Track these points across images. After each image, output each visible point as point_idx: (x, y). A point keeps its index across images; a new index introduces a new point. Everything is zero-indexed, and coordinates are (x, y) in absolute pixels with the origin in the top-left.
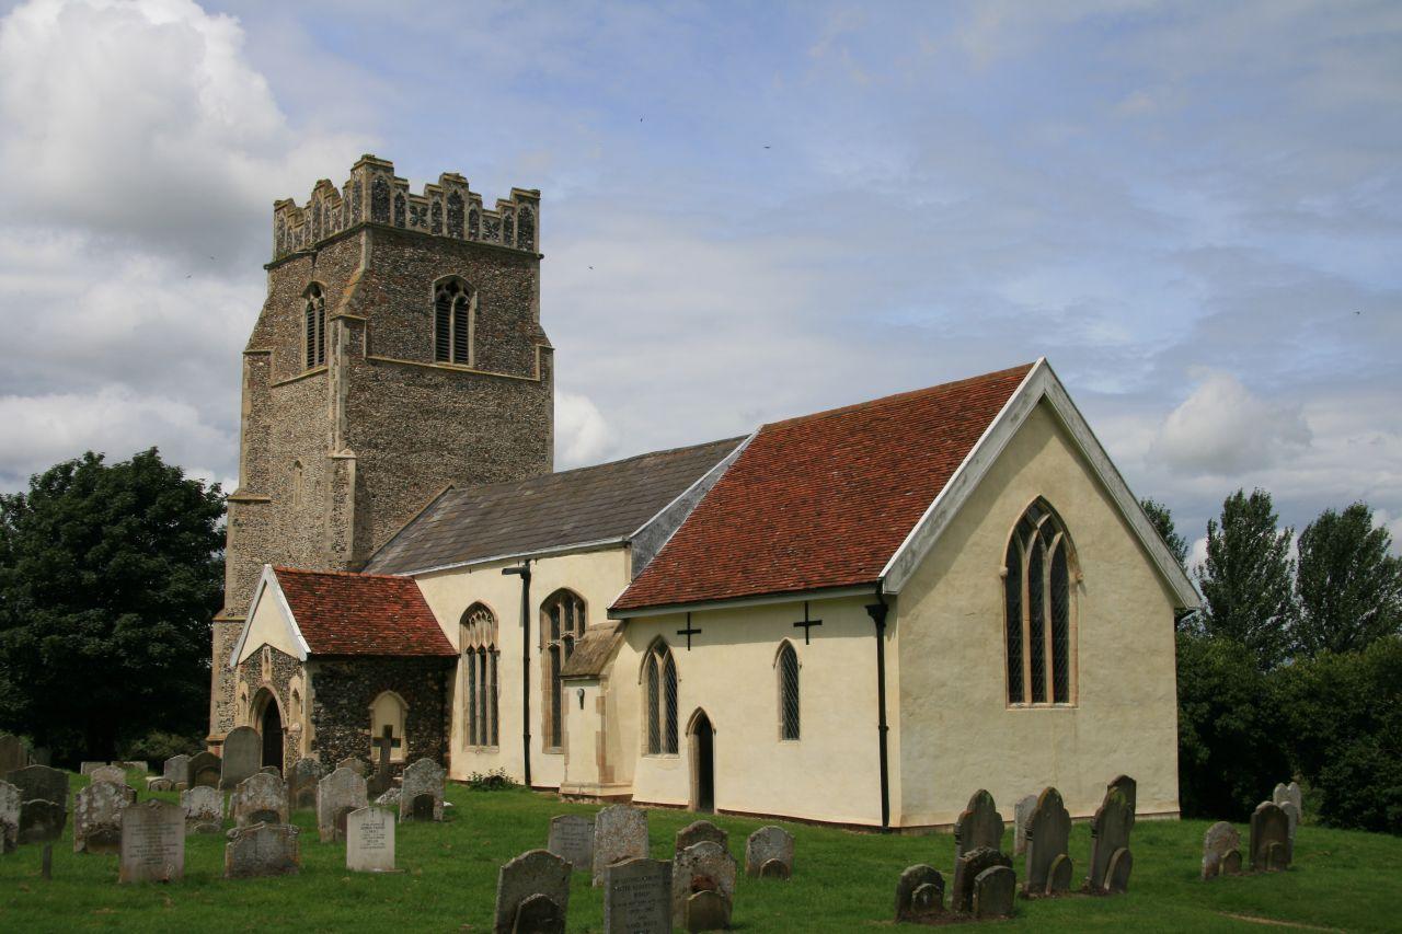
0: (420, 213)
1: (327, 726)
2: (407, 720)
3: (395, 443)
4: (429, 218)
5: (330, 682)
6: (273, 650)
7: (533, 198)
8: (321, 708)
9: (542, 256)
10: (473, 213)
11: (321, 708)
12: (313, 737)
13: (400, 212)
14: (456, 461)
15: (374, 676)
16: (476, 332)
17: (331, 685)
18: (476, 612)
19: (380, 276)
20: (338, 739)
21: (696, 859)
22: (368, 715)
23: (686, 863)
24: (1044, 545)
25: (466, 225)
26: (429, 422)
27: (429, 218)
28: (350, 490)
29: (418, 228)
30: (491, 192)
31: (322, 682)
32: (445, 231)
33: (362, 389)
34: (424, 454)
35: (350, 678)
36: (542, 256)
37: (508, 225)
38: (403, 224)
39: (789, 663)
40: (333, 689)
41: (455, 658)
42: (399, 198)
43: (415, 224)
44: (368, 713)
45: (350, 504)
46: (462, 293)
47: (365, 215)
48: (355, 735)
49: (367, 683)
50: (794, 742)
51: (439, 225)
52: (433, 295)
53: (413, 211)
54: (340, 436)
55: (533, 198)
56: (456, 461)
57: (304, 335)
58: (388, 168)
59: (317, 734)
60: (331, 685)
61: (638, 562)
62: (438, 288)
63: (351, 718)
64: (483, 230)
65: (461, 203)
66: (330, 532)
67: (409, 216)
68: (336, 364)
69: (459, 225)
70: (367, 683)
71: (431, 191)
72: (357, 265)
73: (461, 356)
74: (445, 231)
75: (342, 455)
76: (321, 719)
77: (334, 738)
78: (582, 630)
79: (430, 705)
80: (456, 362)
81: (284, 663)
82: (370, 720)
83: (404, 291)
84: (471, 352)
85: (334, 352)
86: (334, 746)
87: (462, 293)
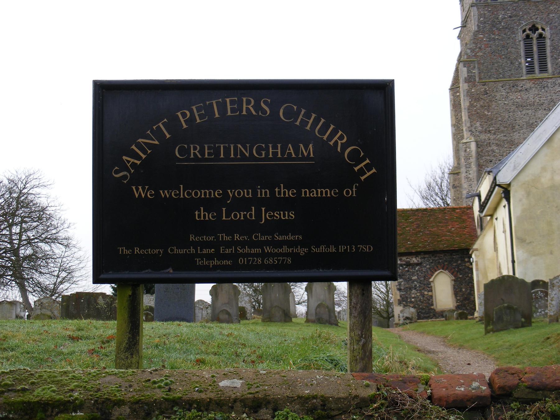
1: (406, 291)
2: (454, 286)
3: (502, 128)
5: (406, 268)
8: (402, 282)
11: (402, 282)
12: (399, 298)
15: (432, 263)
16: (551, 52)
17: (407, 269)
19: (483, 32)
20: (413, 298)
21: (42, 303)
22: (430, 284)
23: (38, 305)
26: (524, 112)
28: (473, 160)
31: (401, 268)
33: (477, 100)
34: (521, 131)
35: (417, 264)
40: (408, 271)
44: (429, 283)
46: (540, 31)
48: (423, 295)
49: (428, 266)
52: (520, 36)
54: (466, 129)
59: (401, 296)
60: (407, 269)
62: (524, 31)
63: (420, 286)
70: (428, 266)
73: (543, 68)
75: (468, 140)
76: (402, 288)
77: (411, 298)
79: (468, 276)
80: (540, 73)
82: (431, 287)
83: (500, 38)
84: (549, 65)
87: (540, 31)
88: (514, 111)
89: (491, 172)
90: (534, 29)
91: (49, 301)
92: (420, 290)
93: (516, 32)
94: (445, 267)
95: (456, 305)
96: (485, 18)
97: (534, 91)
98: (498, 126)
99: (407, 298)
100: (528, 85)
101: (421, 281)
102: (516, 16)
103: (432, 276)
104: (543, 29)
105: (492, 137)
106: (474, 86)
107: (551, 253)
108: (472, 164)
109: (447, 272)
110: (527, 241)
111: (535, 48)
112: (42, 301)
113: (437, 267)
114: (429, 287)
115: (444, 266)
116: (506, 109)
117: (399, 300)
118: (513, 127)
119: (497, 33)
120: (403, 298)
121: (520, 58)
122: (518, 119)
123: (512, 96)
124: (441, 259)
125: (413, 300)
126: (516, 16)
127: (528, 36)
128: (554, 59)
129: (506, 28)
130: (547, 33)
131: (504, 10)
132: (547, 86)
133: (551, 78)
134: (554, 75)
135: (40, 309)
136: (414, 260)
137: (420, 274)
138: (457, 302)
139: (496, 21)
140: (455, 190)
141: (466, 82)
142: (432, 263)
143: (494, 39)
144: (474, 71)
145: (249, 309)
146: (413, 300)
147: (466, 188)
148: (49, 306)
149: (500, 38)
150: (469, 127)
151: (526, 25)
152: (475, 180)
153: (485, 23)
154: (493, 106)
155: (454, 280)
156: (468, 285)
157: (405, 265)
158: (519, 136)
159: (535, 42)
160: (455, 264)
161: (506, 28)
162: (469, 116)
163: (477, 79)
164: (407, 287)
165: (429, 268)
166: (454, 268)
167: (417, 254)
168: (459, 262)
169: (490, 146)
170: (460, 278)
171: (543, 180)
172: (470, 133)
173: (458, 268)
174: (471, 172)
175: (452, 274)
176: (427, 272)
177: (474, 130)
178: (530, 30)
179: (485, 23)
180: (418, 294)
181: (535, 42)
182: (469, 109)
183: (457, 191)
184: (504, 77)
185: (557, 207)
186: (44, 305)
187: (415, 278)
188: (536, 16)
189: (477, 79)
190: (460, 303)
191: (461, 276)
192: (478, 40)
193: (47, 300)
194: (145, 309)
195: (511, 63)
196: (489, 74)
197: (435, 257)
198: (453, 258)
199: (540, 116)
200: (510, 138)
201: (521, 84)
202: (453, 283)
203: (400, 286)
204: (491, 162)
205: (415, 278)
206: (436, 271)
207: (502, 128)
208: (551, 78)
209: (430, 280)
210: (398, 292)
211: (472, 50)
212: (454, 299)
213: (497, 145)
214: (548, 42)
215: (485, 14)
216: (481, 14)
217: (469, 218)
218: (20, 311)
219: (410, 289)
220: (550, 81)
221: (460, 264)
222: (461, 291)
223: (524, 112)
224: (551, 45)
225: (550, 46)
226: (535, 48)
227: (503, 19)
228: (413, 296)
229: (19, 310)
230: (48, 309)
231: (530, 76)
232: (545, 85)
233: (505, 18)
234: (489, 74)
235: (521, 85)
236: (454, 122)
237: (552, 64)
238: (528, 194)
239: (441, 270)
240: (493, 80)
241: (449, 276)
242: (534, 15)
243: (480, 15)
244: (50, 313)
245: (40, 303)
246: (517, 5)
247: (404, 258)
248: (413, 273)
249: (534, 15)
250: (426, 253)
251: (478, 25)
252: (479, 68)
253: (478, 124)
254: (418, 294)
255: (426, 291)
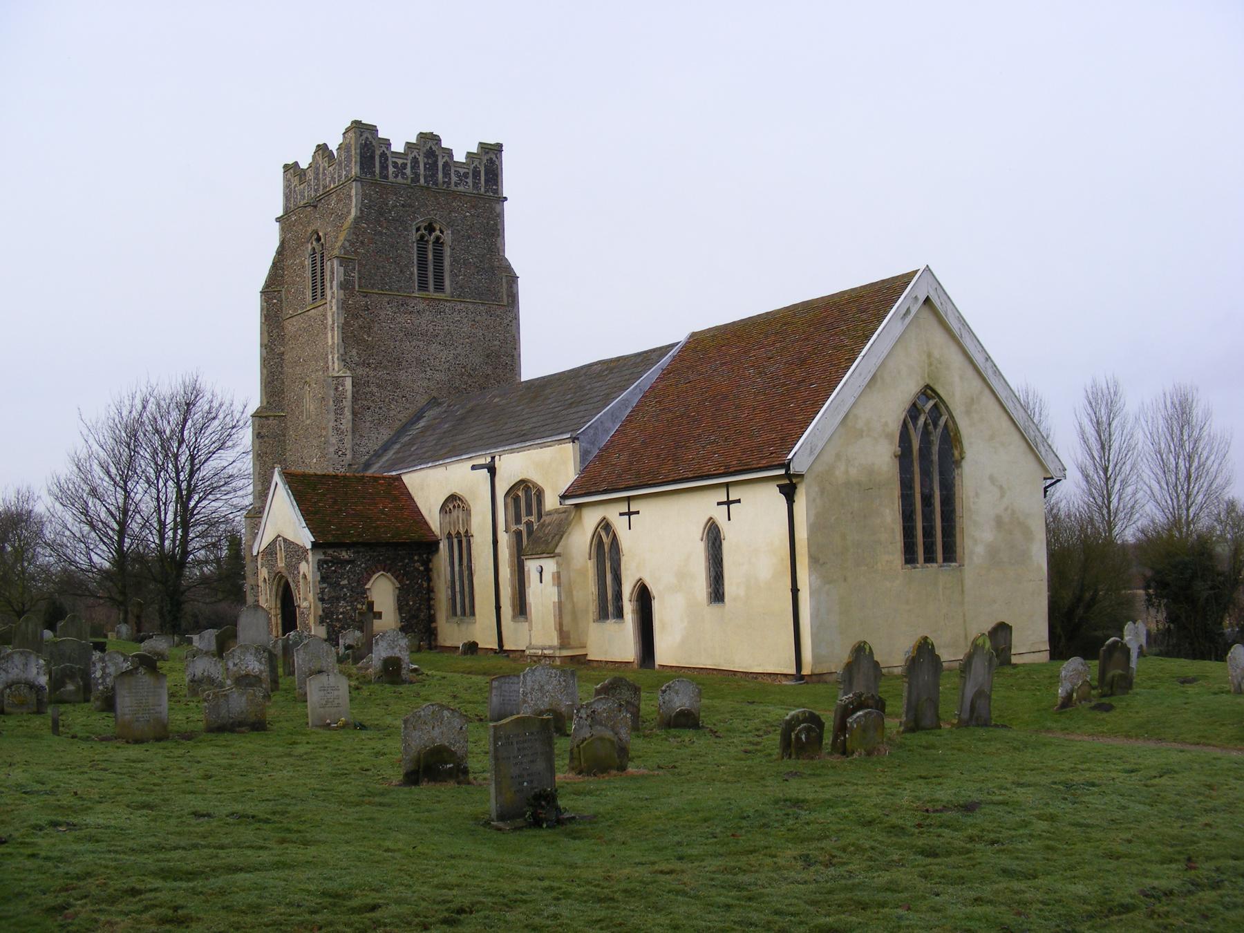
0: (400, 169)
3: (385, 362)
4: (408, 171)
5: (332, 566)
6: (285, 540)
7: (498, 148)
8: (326, 588)
9: (506, 199)
10: (446, 165)
11: (326, 588)
13: (384, 167)
14: (437, 376)
15: (369, 560)
16: (451, 265)
18: (453, 503)
20: (341, 613)
21: (594, 712)
22: (365, 593)
23: (585, 716)
24: (931, 427)
25: (440, 175)
26: (414, 344)
27: (408, 171)
28: (347, 403)
29: (400, 180)
30: (460, 146)
31: (325, 566)
32: (422, 181)
34: (410, 370)
35: (349, 562)
36: (506, 199)
37: (476, 174)
38: (386, 177)
39: (714, 537)
40: (335, 571)
41: (431, 546)
42: (383, 155)
43: (396, 176)
45: (348, 413)
46: (438, 233)
47: (355, 170)
50: (720, 604)
51: (417, 175)
52: (414, 236)
53: (395, 165)
55: (498, 148)
56: (437, 376)
57: (308, 274)
58: (373, 129)
59: (323, 611)
61: (584, 454)
62: (418, 229)
64: (454, 179)
65: (387, 159)
66: (333, 440)
67: (391, 169)
68: (333, 297)
69: (434, 175)
71: (469, 155)
72: (349, 212)
73: (439, 287)
74: (422, 181)
75: (341, 374)
76: (326, 598)
78: (540, 516)
80: (435, 292)
81: (296, 553)
83: (389, 233)
84: (447, 283)
85: (331, 288)
86: (338, 620)
87: (438, 233)
88: (401, 341)
89: (578, 439)
90: (431, 229)
91: (610, 707)
92: (352, 602)
93: (410, 228)
94: (387, 568)
95: (399, 625)
96: (370, 201)
97: (427, 316)
98: (381, 358)
99: (332, 613)
100: (421, 306)
101: (353, 587)
102: (411, 206)
103: (369, 580)
104: (442, 232)
105: (372, 373)
106: (352, 295)
107: (845, 580)
108: (346, 409)
109: (389, 575)
110: (821, 561)
111: (430, 256)
112: (595, 706)
113: (376, 568)
114: (364, 598)
115: (385, 566)
116: (392, 336)
117: (320, 616)
118: (399, 364)
119: (385, 225)
120: (327, 613)
121: (413, 267)
122: (406, 352)
123: (401, 319)
124: (381, 555)
125: (341, 616)
126: (411, 206)
127: (422, 237)
128: (454, 275)
129: (397, 220)
130: (447, 237)
131: (396, 194)
132: (444, 312)
133: (449, 301)
134: (453, 297)
135: (590, 726)
136: (345, 555)
137: (352, 577)
138: (401, 622)
139: (385, 208)
140: (260, 440)
141: (341, 289)
142: (369, 560)
143: (381, 233)
144: (353, 275)
145: (406, 661)
146: (341, 616)
147: (334, 444)
148: (608, 717)
149: (389, 233)
150: (342, 355)
151: (422, 221)
152: (350, 433)
153: (370, 207)
154: (376, 329)
155: (399, 589)
156: (417, 596)
157: (331, 561)
158: (407, 376)
159: (430, 246)
160: (400, 564)
161: (397, 220)
162: (343, 338)
163: (357, 287)
164: (333, 597)
165: (365, 569)
166: (400, 570)
167: (347, 546)
168: (407, 561)
169: (369, 387)
170: (407, 585)
171: (837, 473)
172: (343, 363)
173: (404, 570)
174: (343, 421)
175: (396, 578)
176: (363, 574)
177: (348, 360)
178: (425, 229)
179: (370, 207)
180: (348, 608)
181: (430, 246)
182: (343, 328)
183: (265, 442)
184: (391, 290)
185: (852, 513)
186: (598, 717)
187: (345, 582)
188: (435, 212)
189: (357, 287)
190: (406, 623)
191: (408, 582)
192: (360, 229)
193: (604, 705)
194: (801, 718)
195: (401, 271)
196: (372, 281)
197: (374, 552)
198: (399, 555)
199: (433, 351)
200: (395, 378)
201: (412, 303)
202: (397, 591)
203: (322, 595)
204: (369, 409)
205: (345, 582)
206: (374, 573)
207: (385, 362)
208: (449, 301)
209: (366, 587)
210: (320, 604)
211: (352, 244)
212: (398, 616)
213: (378, 386)
214: (447, 251)
215: (370, 196)
216: (366, 195)
217: (402, 494)
218: (38, 673)
219: (338, 599)
220: (449, 304)
221: (407, 564)
222: (407, 604)
223: (414, 344)
224: (451, 256)
225: (451, 257)
226: (430, 256)
227: (393, 207)
228: (341, 610)
229: (35, 671)
230: (606, 726)
231: (423, 294)
232: (442, 310)
233: (396, 206)
234: (372, 281)
235: (413, 305)
236: (266, 341)
237: (452, 281)
238: (822, 491)
239: (382, 572)
240: (376, 291)
241: (390, 580)
242: (433, 210)
243: (365, 196)
244: (611, 733)
245: (589, 712)
246: (412, 190)
247: (330, 552)
248: (342, 575)
249: (433, 210)
250: (369, 545)
251: (361, 209)
252: (359, 271)
253: (354, 352)
254: (348, 608)
255: (359, 603)
